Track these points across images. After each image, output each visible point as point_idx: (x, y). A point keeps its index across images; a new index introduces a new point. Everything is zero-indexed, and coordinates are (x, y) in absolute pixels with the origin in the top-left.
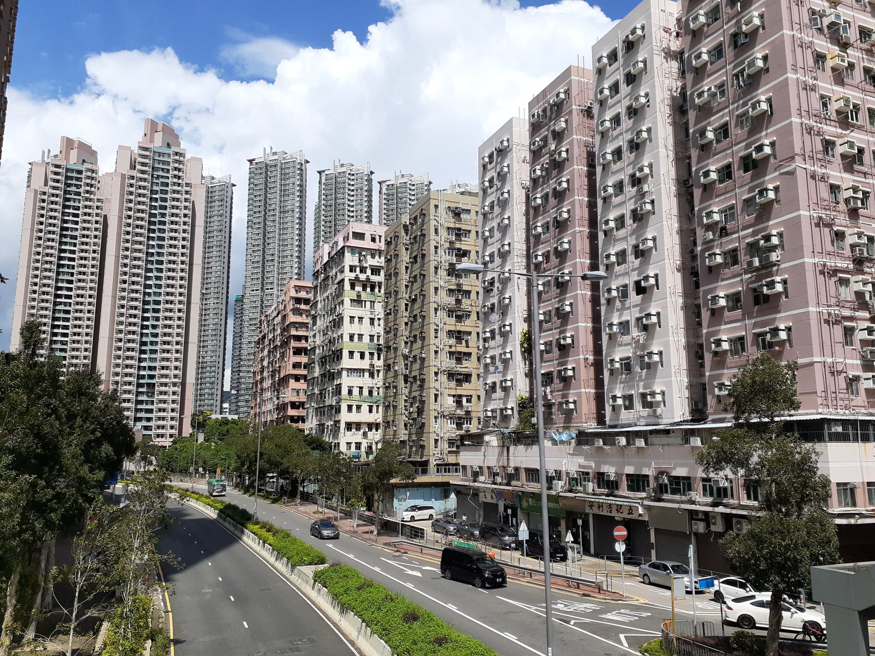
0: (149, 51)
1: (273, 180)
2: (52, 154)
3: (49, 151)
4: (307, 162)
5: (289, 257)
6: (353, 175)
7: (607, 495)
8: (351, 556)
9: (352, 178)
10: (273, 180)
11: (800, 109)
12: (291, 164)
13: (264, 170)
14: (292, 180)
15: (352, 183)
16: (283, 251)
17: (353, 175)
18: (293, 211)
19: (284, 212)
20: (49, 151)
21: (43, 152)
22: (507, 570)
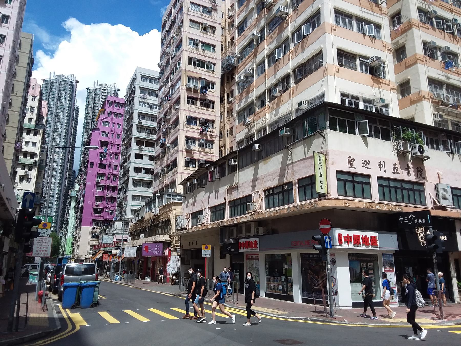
0: (89, 24)
1: (53, 90)
2: (56, 75)
3: (54, 73)
4: (77, 82)
5: (59, 136)
6: (105, 90)
7: (398, 41)
8: (71, 276)
9: (105, 92)
10: (53, 90)
11: (205, 29)
12: (66, 82)
13: (49, 85)
14: (65, 91)
15: (104, 95)
16: (56, 132)
17: (105, 90)
18: (64, 109)
19: (59, 109)
20: (54, 73)
21: (51, 73)
22: (421, 24)
